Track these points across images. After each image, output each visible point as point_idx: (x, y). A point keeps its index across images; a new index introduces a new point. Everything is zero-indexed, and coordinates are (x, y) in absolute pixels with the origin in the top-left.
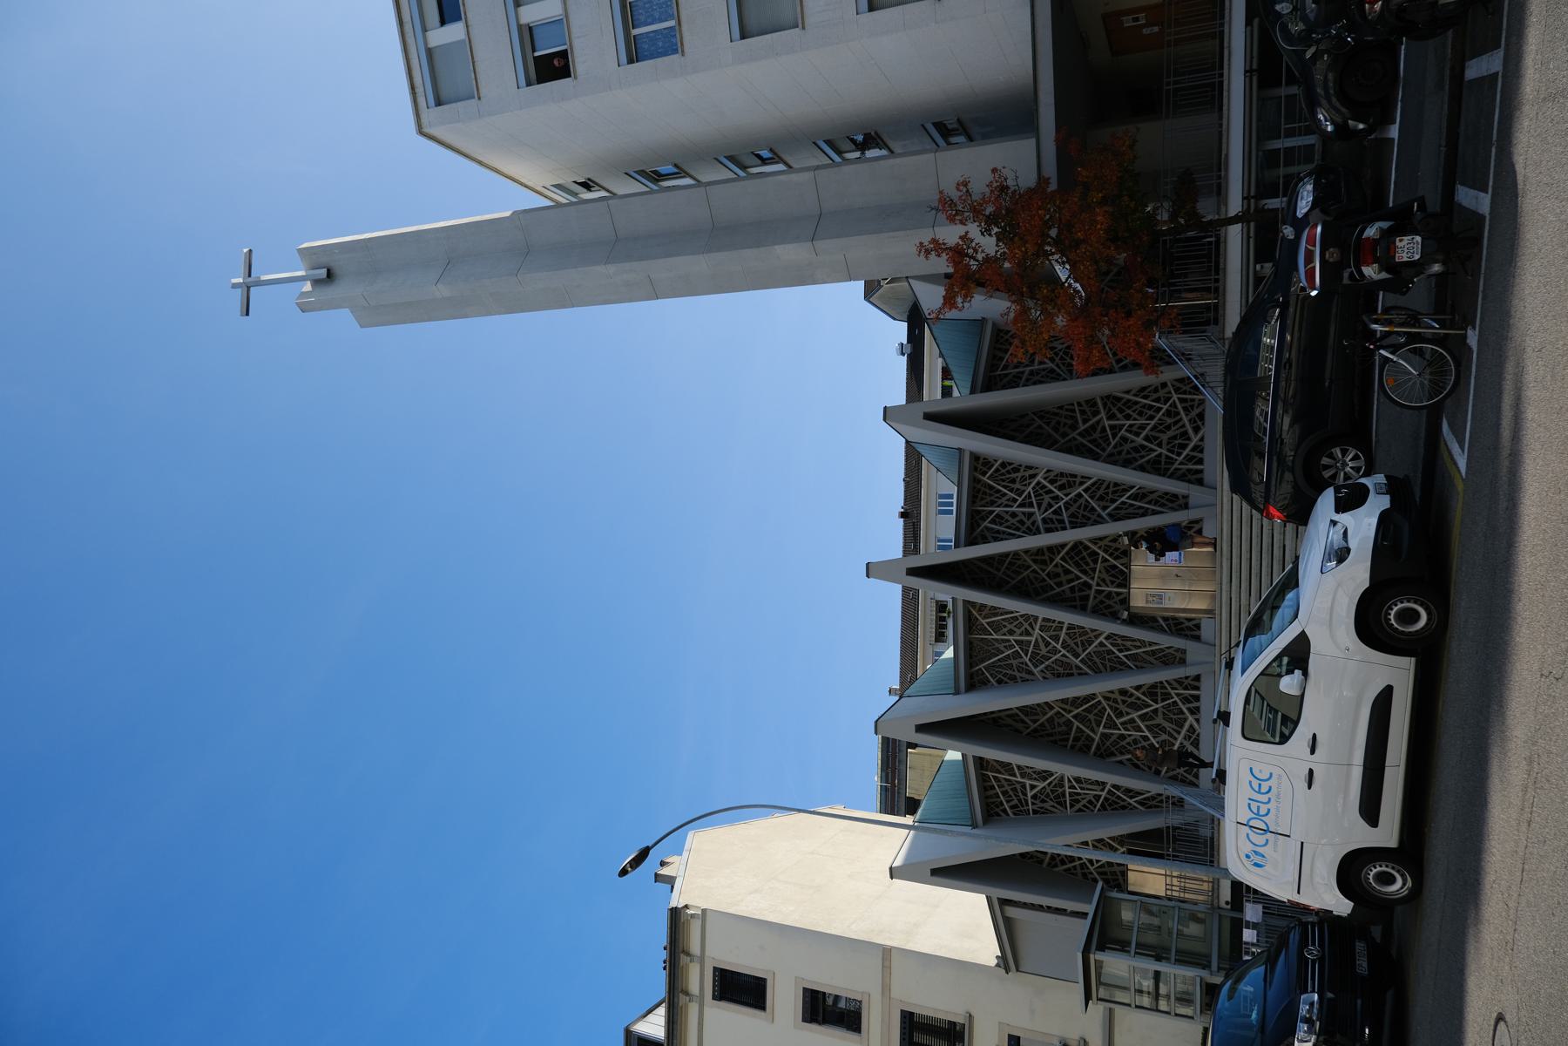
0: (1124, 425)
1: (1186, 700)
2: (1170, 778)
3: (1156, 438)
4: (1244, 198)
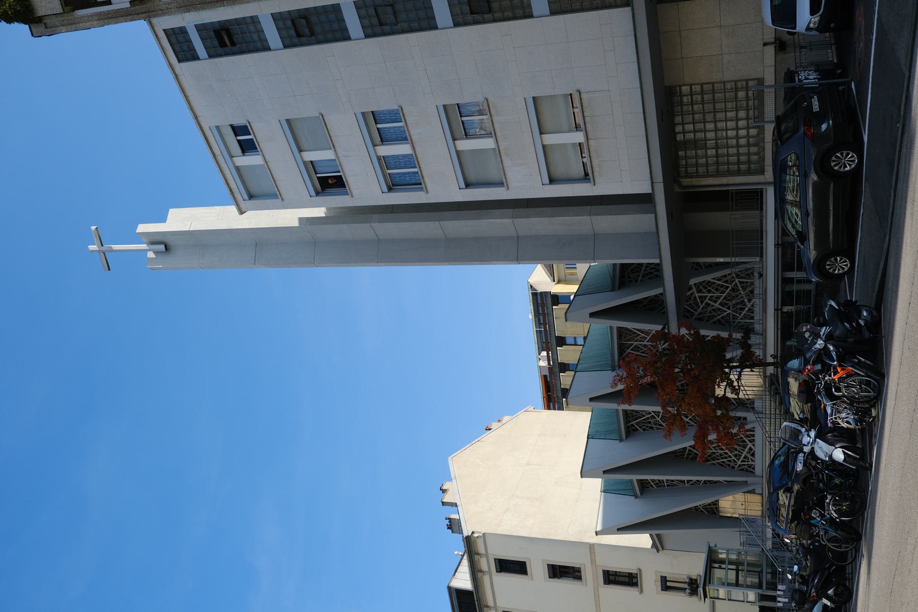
0: (707, 296)
1: (747, 436)
2: (740, 470)
3: (727, 304)
4: (775, 310)
